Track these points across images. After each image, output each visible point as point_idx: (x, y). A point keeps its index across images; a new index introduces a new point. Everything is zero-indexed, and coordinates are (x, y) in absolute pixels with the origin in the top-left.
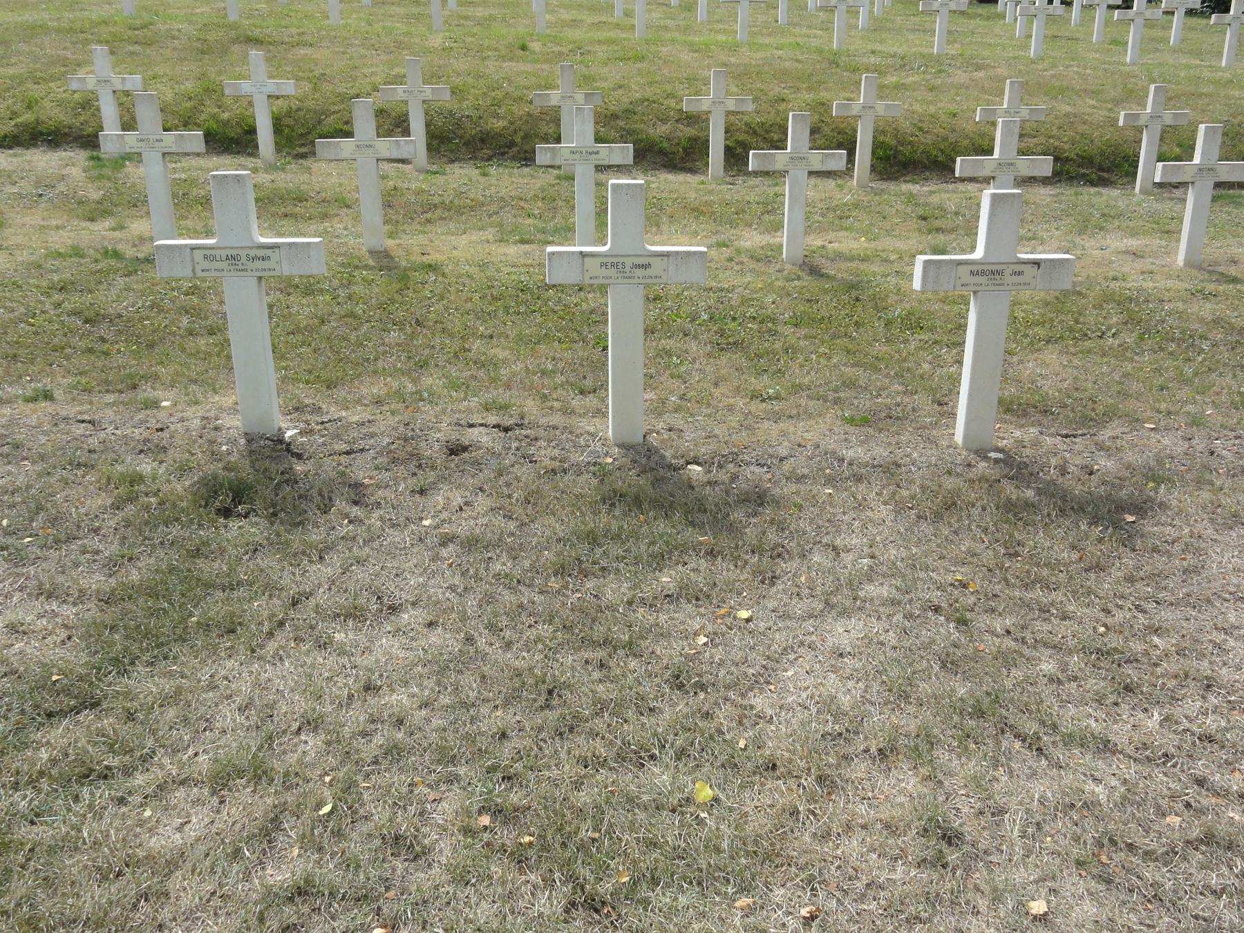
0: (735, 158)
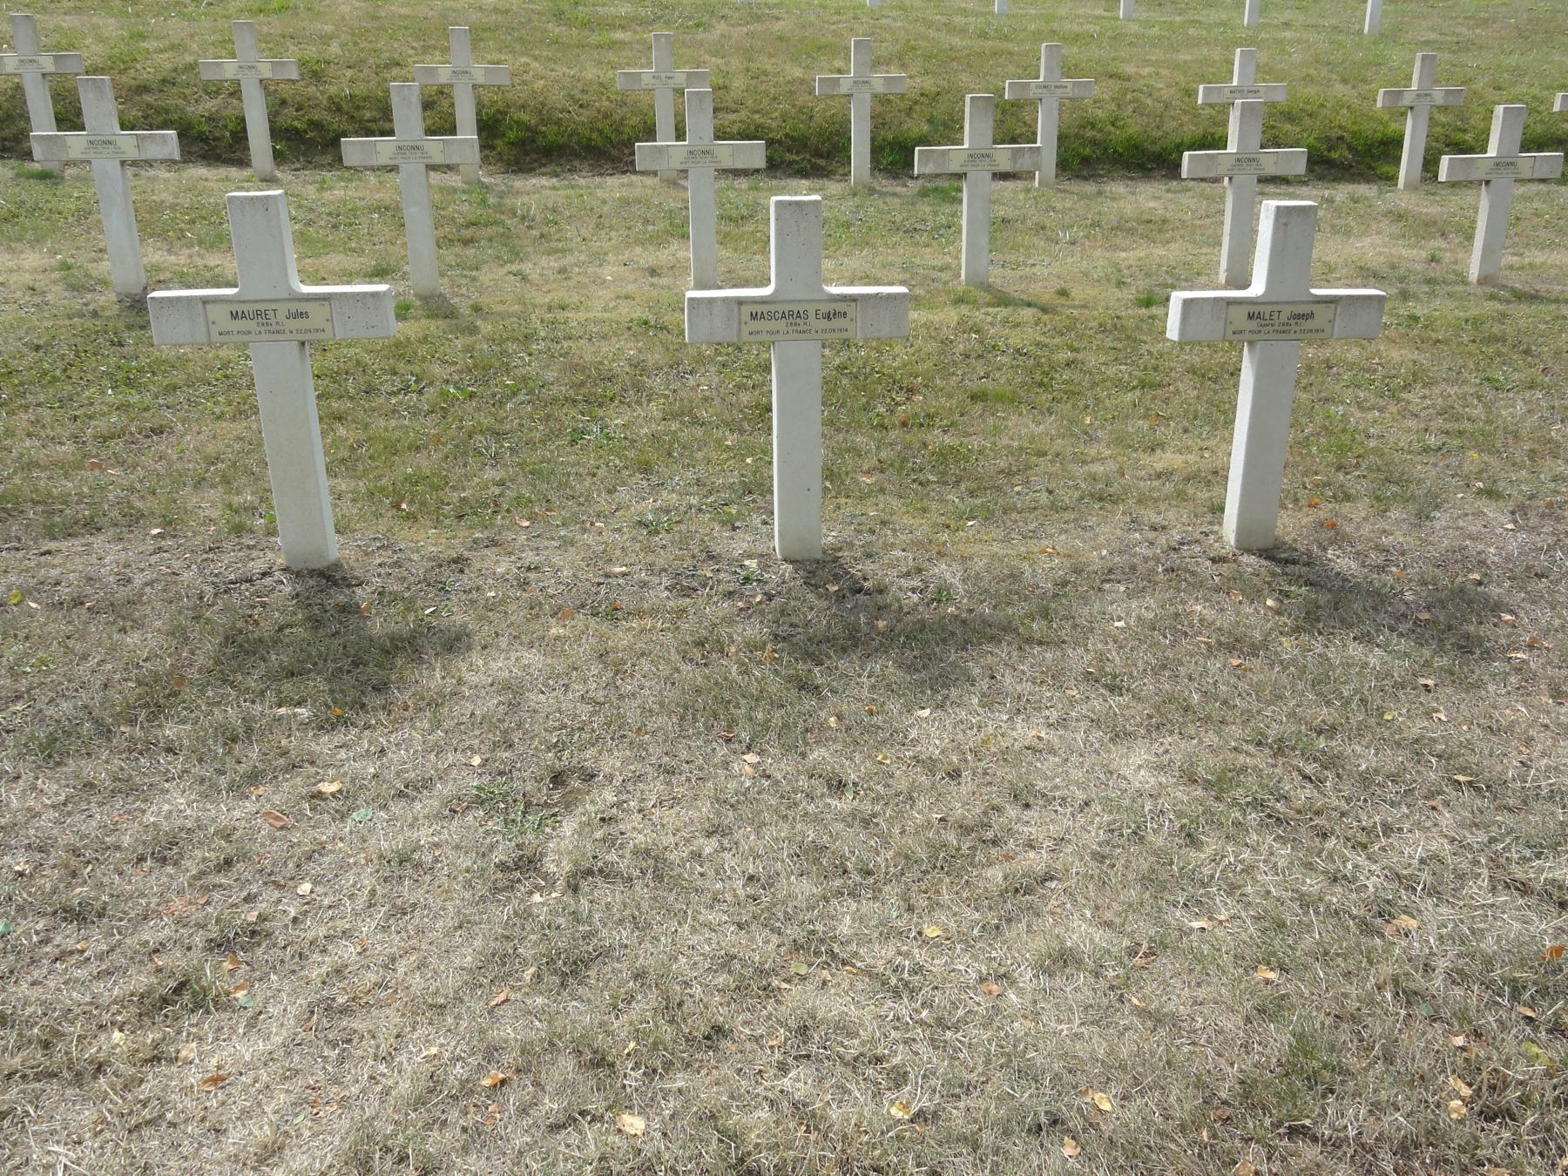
0: (894, 157)
